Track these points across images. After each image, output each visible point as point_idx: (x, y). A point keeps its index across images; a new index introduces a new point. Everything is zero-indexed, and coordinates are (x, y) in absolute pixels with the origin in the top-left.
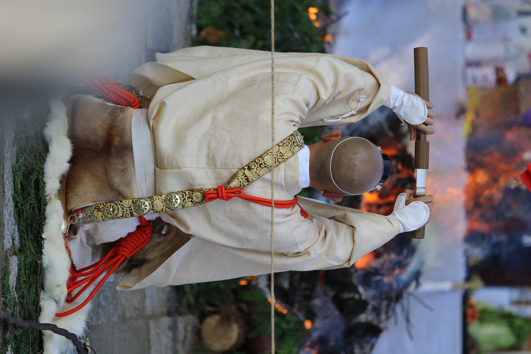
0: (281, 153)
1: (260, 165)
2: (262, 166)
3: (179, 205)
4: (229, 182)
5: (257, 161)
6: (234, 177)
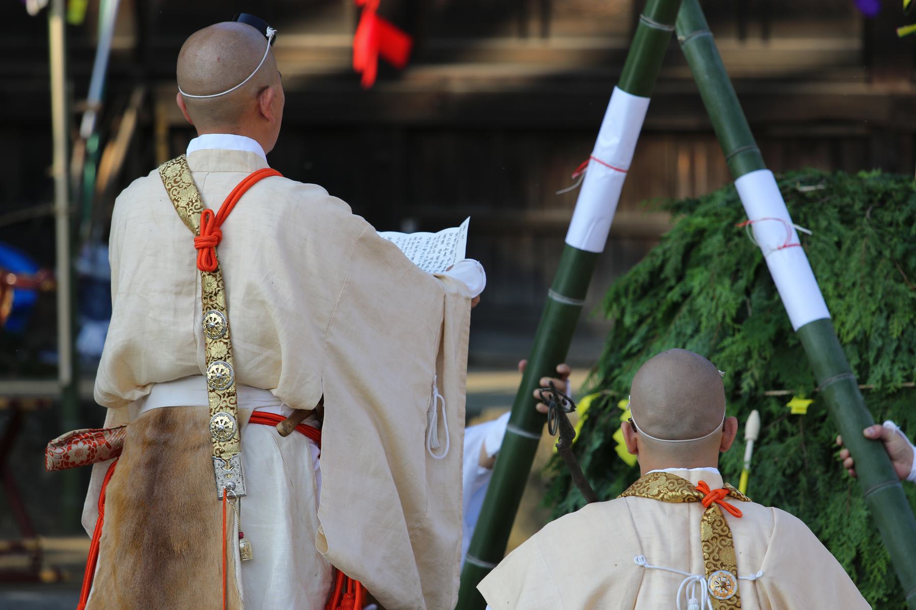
0: (188, 204)
1: (175, 182)
2: (178, 179)
3: (219, 315)
4: (193, 230)
5: (170, 187)
6: (186, 221)
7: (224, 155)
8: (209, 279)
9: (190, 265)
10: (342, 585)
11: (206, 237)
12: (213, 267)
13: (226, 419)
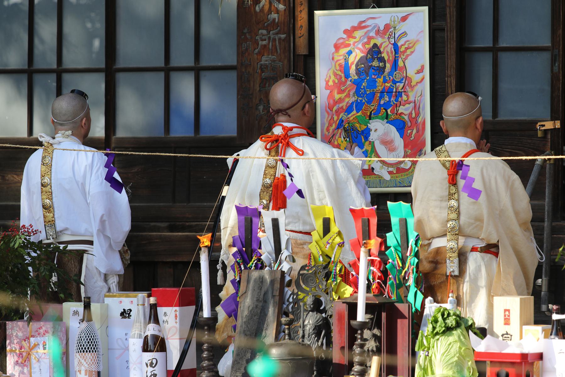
4: (446, 168)
7: (458, 145)
8: (452, 187)
9: (446, 189)
10: (154, 316)
11: (452, 170)
12: (454, 182)
13: (454, 244)
